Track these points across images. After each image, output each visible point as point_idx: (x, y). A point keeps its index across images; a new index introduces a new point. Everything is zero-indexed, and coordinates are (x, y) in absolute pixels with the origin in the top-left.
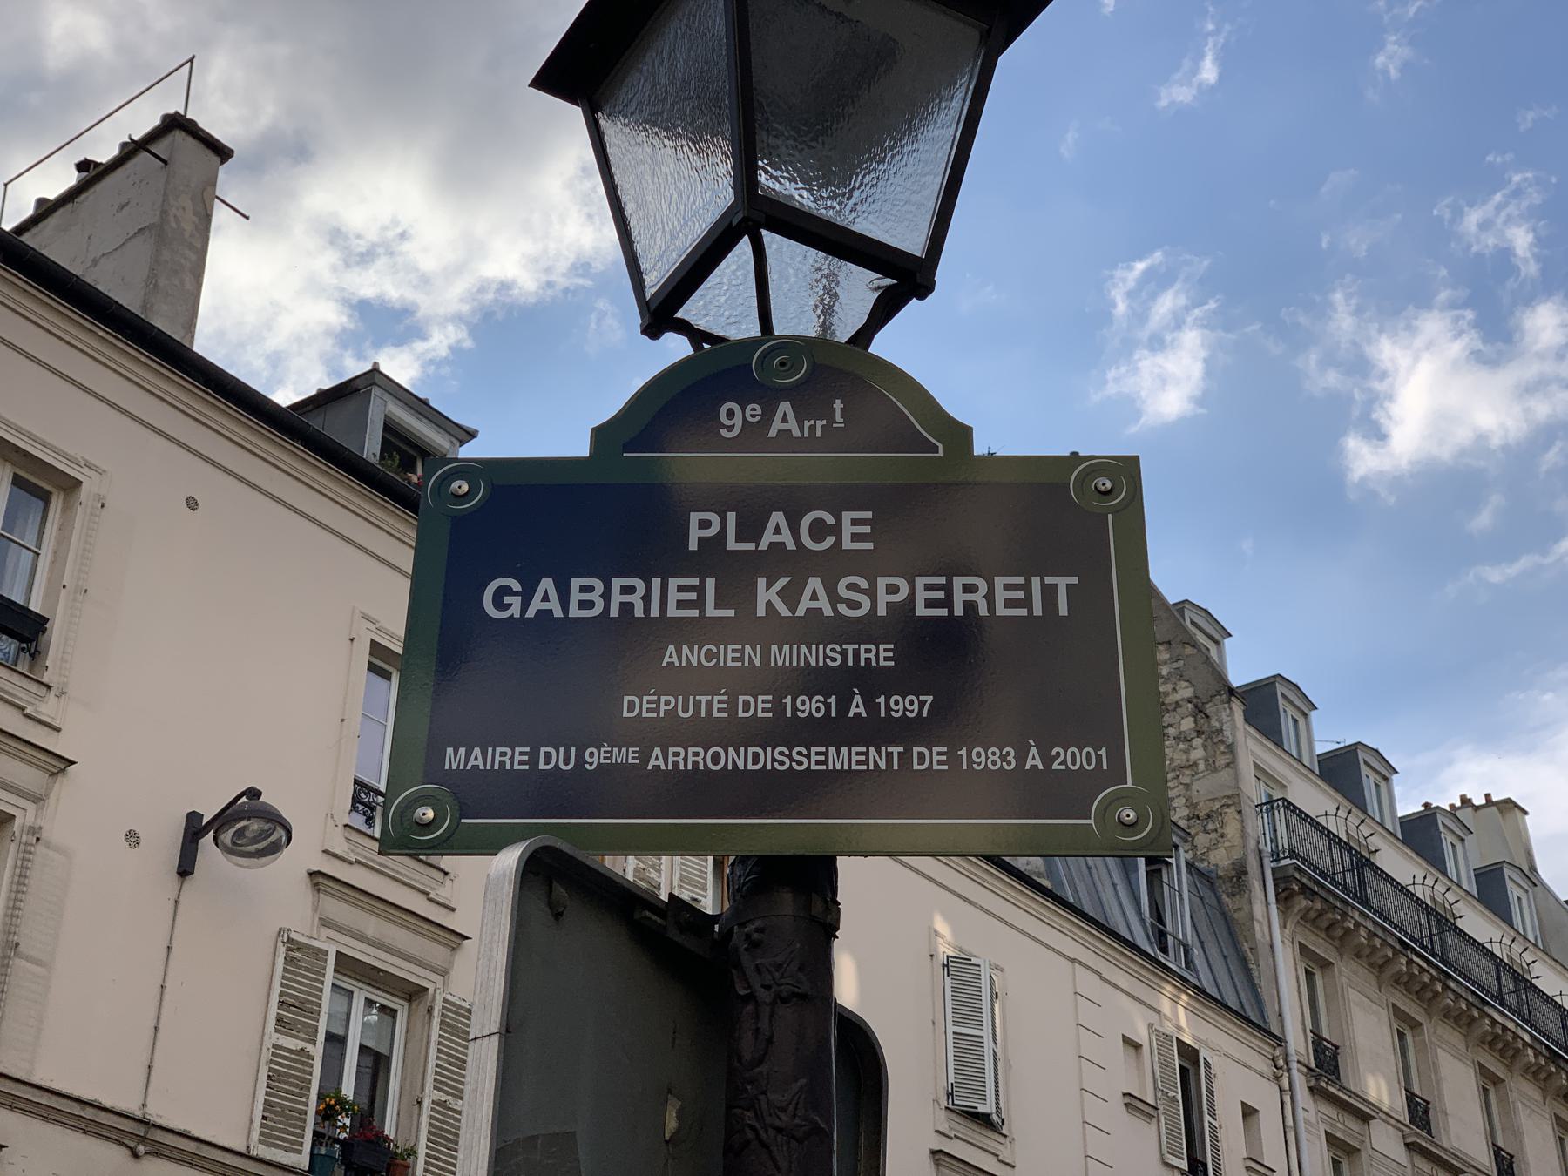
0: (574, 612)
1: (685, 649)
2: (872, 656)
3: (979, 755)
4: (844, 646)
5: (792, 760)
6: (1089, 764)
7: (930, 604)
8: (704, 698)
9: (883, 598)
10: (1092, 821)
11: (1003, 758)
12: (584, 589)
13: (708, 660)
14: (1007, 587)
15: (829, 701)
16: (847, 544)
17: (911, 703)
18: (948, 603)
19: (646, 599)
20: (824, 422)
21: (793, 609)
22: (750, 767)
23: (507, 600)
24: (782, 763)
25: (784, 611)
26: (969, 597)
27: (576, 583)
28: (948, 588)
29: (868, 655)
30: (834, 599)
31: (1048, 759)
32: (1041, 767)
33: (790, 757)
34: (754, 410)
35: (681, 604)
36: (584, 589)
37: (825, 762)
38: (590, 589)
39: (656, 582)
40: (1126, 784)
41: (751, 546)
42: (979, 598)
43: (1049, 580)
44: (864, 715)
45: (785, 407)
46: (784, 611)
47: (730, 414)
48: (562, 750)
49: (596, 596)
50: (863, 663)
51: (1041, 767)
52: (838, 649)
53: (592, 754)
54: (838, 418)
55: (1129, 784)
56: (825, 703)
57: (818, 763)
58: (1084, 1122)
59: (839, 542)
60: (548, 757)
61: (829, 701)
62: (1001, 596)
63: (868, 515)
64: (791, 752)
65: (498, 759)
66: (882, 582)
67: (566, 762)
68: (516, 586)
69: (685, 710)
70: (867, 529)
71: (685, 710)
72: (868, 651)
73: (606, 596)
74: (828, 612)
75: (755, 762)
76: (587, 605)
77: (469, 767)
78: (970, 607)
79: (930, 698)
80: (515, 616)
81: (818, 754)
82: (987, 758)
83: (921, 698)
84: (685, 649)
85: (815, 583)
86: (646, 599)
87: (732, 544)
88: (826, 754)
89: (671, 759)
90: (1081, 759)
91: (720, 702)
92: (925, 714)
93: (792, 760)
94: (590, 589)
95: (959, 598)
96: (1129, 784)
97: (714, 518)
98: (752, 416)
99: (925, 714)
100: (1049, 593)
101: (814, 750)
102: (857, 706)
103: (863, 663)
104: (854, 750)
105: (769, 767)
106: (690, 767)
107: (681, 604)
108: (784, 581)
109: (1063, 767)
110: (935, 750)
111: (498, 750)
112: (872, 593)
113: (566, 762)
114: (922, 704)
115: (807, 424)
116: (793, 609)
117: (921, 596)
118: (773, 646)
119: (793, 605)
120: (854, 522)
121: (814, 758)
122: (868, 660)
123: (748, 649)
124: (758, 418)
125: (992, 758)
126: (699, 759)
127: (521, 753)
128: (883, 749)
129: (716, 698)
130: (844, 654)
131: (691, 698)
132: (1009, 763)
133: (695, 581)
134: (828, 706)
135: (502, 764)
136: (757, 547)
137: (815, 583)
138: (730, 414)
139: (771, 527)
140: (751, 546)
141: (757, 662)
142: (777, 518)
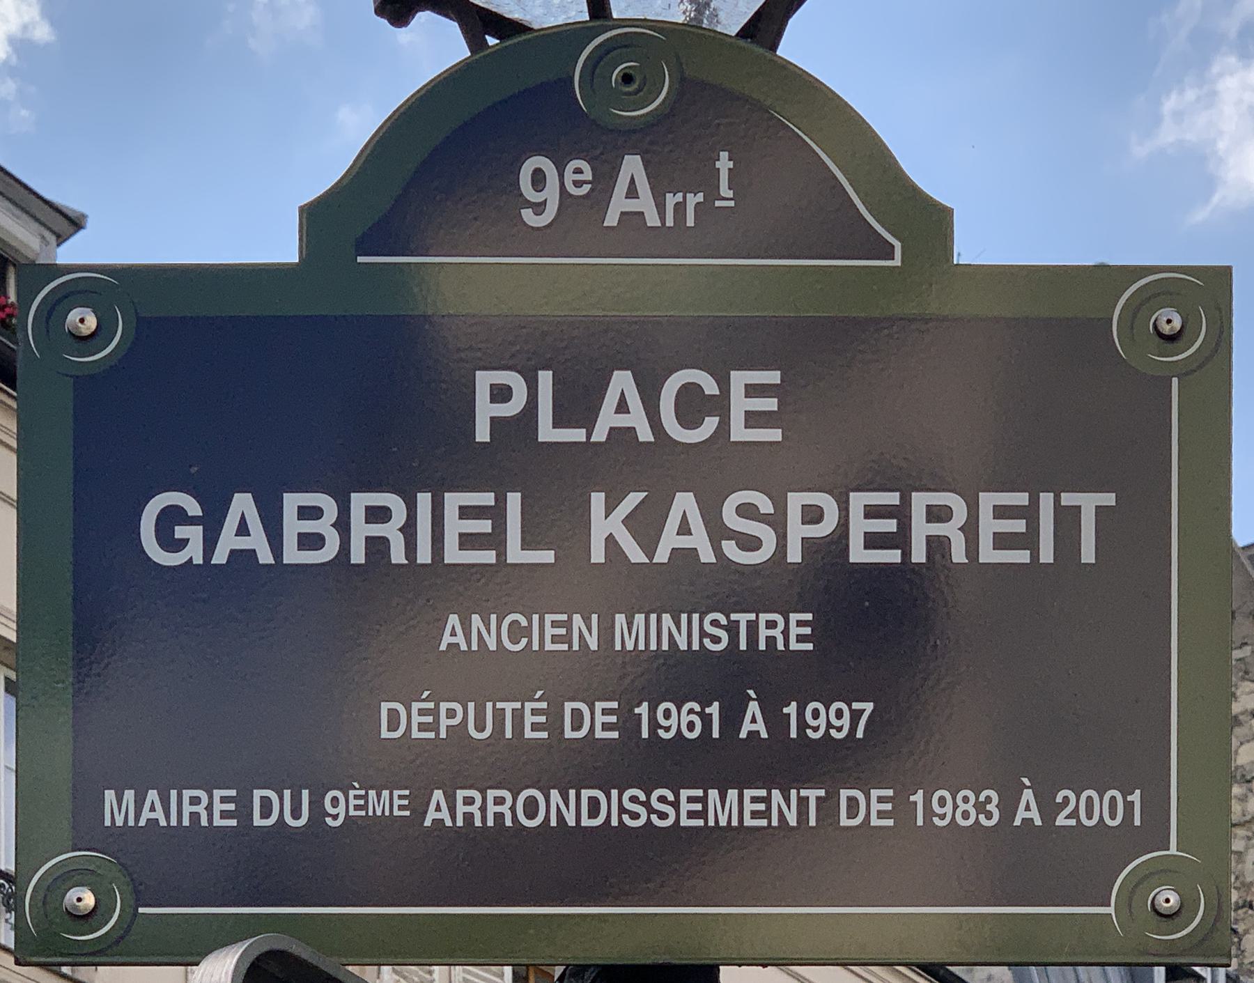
3: (942, 802)
4: (734, 617)
5: (651, 810)
6: (1113, 817)
8: (509, 707)
9: (797, 531)
10: (1111, 910)
11: (981, 807)
15: (708, 710)
16: (739, 432)
17: (839, 714)
19: (409, 530)
22: (586, 822)
23: (180, 532)
25: (636, 555)
28: (902, 513)
30: (718, 531)
31: (1049, 808)
32: (1038, 822)
33: (647, 805)
41: (578, 435)
45: (632, 166)
46: (636, 555)
48: (287, 793)
49: (324, 526)
50: (762, 646)
51: (1038, 822)
52: (724, 621)
55: (1173, 850)
59: (724, 426)
61: (708, 710)
65: (187, 809)
66: (796, 501)
67: (296, 814)
71: (480, 728)
72: (771, 625)
73: (343, 525)
75: (594, 813)
77: (142, 823)
79: (868, 707)
82: (955, 807)
87: (547, 432)
88: (704, 800)
89: (461, 809)
90: (1101, 808)
91: (534, 712)
92: (860, 734)
93: (651, 810)
95: (921, 530)
96: (1173, 850)
99: (860, 734)
101: (685, 794)
102: (754, 720)
103: (762, 646)
104: (748, 793)
105: (615, 822)
108: (633, 499)
109: (1073, 822)
112: (778, 522)
113: (296, 814)
114: (856, 715)
115: (671, 200)
117: (859, 527)
119: (648, 537)
121: (685, 807)
122: (771, 640)
125: (962, 807)
128: (793, 792)
129: (529, 706)
130: (732, 629)
132: (989, 816)
134: (706, 720)
135: (195, 817)
138: (335, 801)
140: (578, 435)
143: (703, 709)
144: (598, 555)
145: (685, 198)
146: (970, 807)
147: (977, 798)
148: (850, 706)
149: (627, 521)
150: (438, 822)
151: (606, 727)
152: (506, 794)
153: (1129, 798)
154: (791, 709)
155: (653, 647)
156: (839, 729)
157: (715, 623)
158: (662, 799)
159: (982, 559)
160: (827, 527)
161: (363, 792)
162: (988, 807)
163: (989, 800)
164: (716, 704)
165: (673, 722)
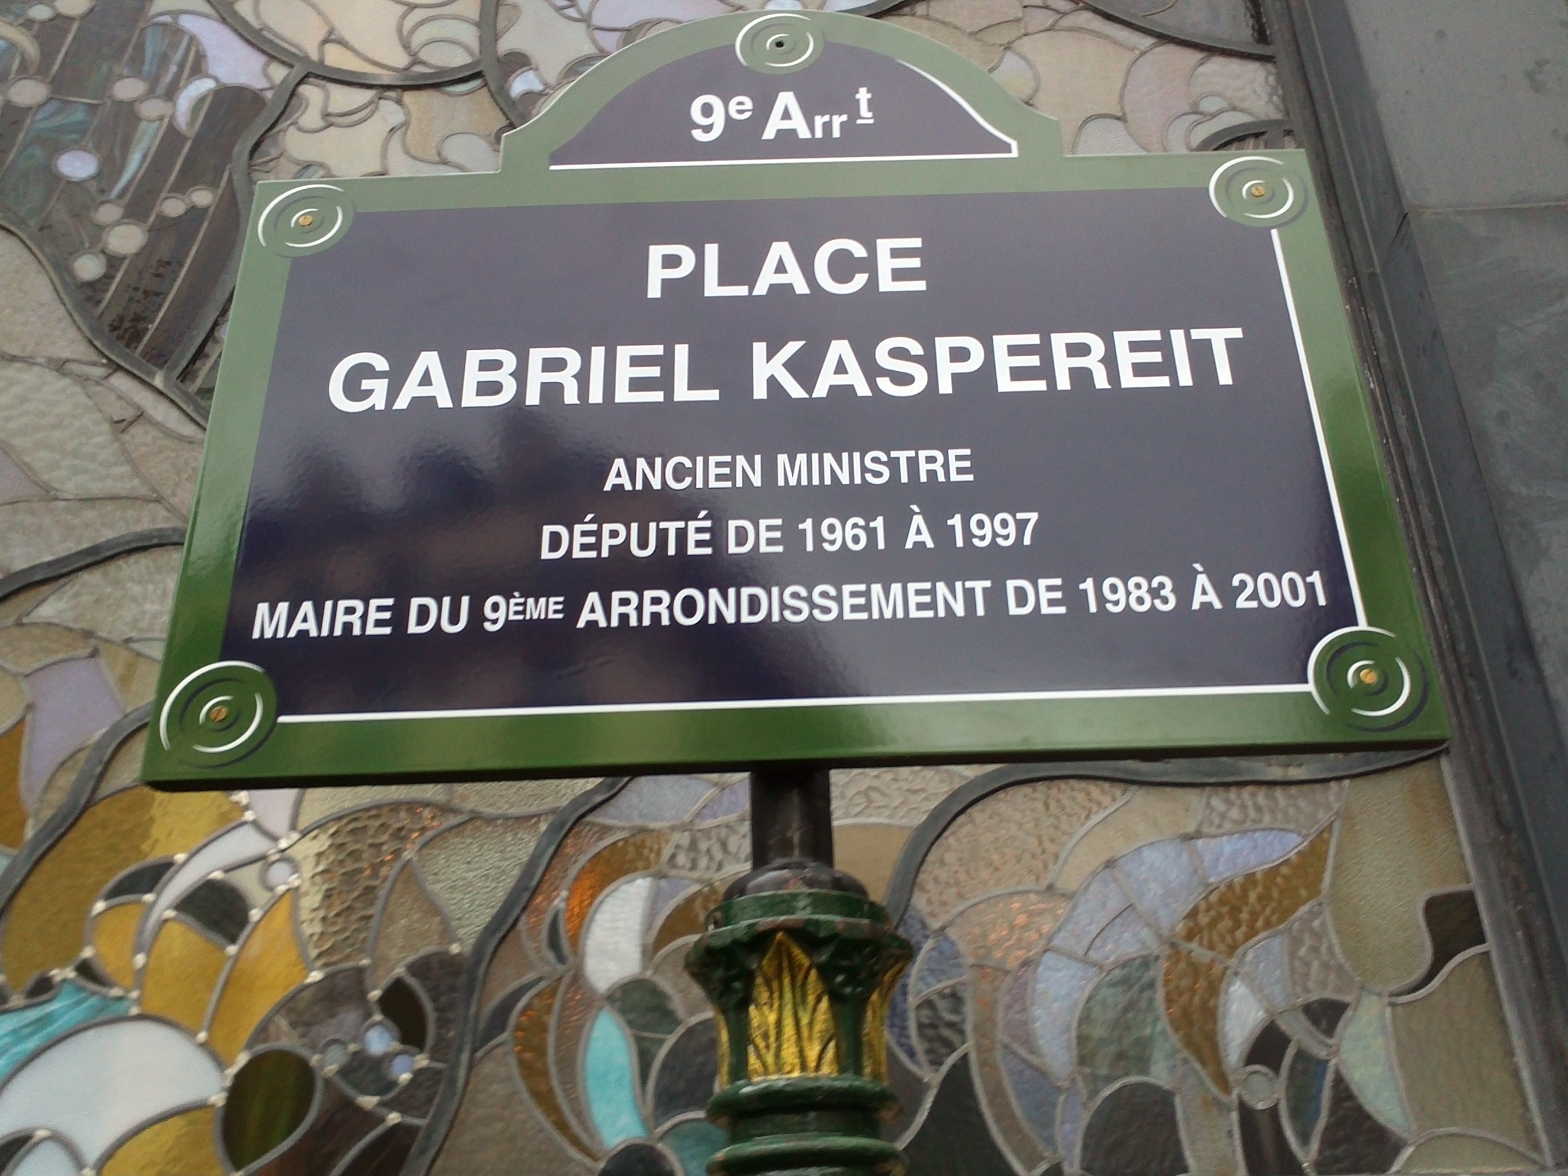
0: (470, 399)
1: (641, 464)
2: (937, 466)
3: (1114, 589)
4: (894, 454)
5: (813, 606)
6: (1296, 597)
7: (1017, 374)
8: (672, 526)
9: (946, 369)
10: (1310, 687)
11: (1155, 593)
12: (487, 365)
13: (678, 479)
14: (1135, 347)
15: (872, 524)
16: (886, 284)
17: (1004, 524)
18: (1046, 371)
19: (583, 378)
20: (844, 118)
21: (809, 388)
22: (746, 618)
23: (366, 384)
24: (797, 611)
25: (796, 391)
26: (1078, 362)
27: (473, 357)
28: (1044, 350)
29: (931, 467)
30: (872, 371)
31: (1229, 594)
32: (1218, 605)
33: (809, 600)
34: (742, 106)
35: (637, 384)
36: (487, 365)
37: (867, 607)
38: (496, 365)
39: (598, 354)
40: (1356, 624)
41: (742, 291)
42: (1093, 362)
43: (1197, 334)
44: (930, 544)
45: (786, 99)
46: (796, 391)
47: (707, 110)
48: (446, 601)
49: (503, 376)
50: (923, 478)
51: (1218, 605)
52: (884, 457)
53: (495, 607)
54: (864, 111)
55: (1363, 625)
56: (866, 528)
57: (855, 608)
58: (973, 34)
59: (873, 280)
60: (423, 614)
61: (872, 524)
62: (1126, 359)
63: (916, 243)
64: (810, 593)
65: (341, 618)
66: (943, 345)
67: (454, 619)
68: (380, 363)
69: (643, 545)
70: (915, 263)
71: (643, 545)
72: (931, 460)
73: (520, 375)
74: (863, 390)
75: (754, 609)
76: (493, 388)
77: (292, 634)
78: (1082, 376)
79: (1033, 517)
80: (377, 408)
81: (853, 594)
82: (1128, 593)
83: (1020, 516)
84: (641, 464)
85: (840, 349)
86: (583, 378)
87: (712, 288)
88: (867, 594)
89: (616, 610)
90: (1282, 590)
91: (699, 530)
92: (1027, 541)
93: (813, 606)
94: (496, 365)
95: (1063, 365)
96: (1363, 625)
97: (687, 255)
98: (741, 112)
99: (1027, 541)
100: (1201, 353)
101: (847, 589)
102: (919, 532)
103: (923, 478)
104: (912, 587)
105: (776, 618)
106: (646, 622)
107: (637, 384)
108: (792, 347)
109: (1254, 604)
110: (1043, 583)
111: (343, 604)
112: (929, 361)
113: (454, 619)
114: (1021, 525)
115: (819, 121)
116: (809, 386)
117: (1004, 363)
118: (780, 457)
119: (808, 380)
120: (896, 253)
121: (848, 601)
122: (932, 474)
123: (741, 460)
124: (747, 115)
125: (1135, 593)
126: (662, 609)
127: (380, 609)
128: (958, 585)
129: (692, 525)
130: (893, 465)
131: (653, 526)
132: (1165, 601)
133: (658, 350)
134: (872, 533)
135: (348, 626)
136: (751, 289)
137: (840, 349)
138: (707, 110)
139: (770, 263)
140: (742, 291)
141: (757, 480)
142: (781, 250)
143: (867, 524)
144: (760, 392)
145: (831, 118)
146: (1143, 593)
147: (1150, 584)
148: (1014, 517)
149: (788, 365)
150: (592, 624)
151: (770, 542)
152: (664, 595)
153: (1309, 579)
154: (956, 521)
155: (816, 481)
156: (1006, 537)
157: (876, 460)
158: (824, 595)
159: (1124, 385)
160: (975, 362)
161: (522, 600)
162: (1163, 593)
163: (1162, 586)
164: (880, 519)
165: (838, 535)
